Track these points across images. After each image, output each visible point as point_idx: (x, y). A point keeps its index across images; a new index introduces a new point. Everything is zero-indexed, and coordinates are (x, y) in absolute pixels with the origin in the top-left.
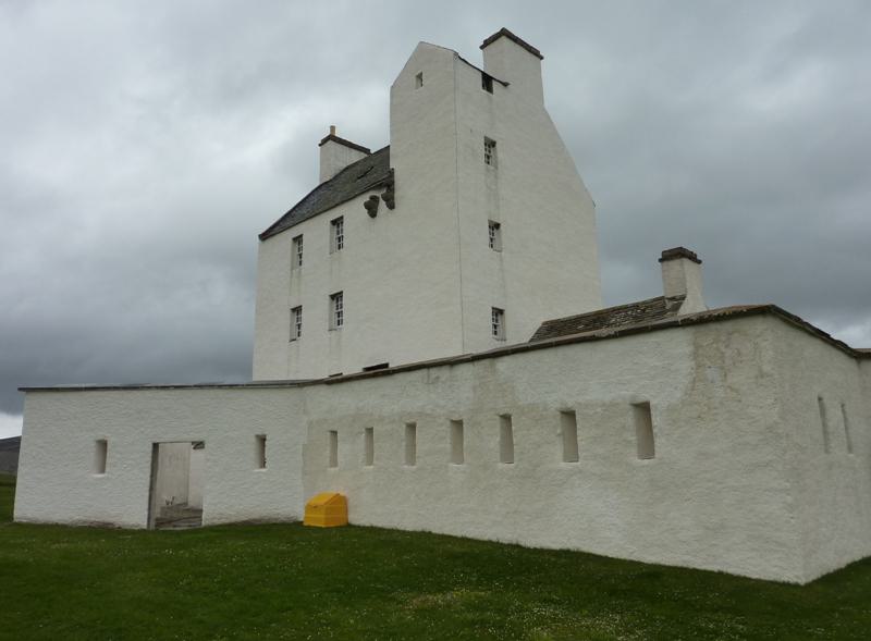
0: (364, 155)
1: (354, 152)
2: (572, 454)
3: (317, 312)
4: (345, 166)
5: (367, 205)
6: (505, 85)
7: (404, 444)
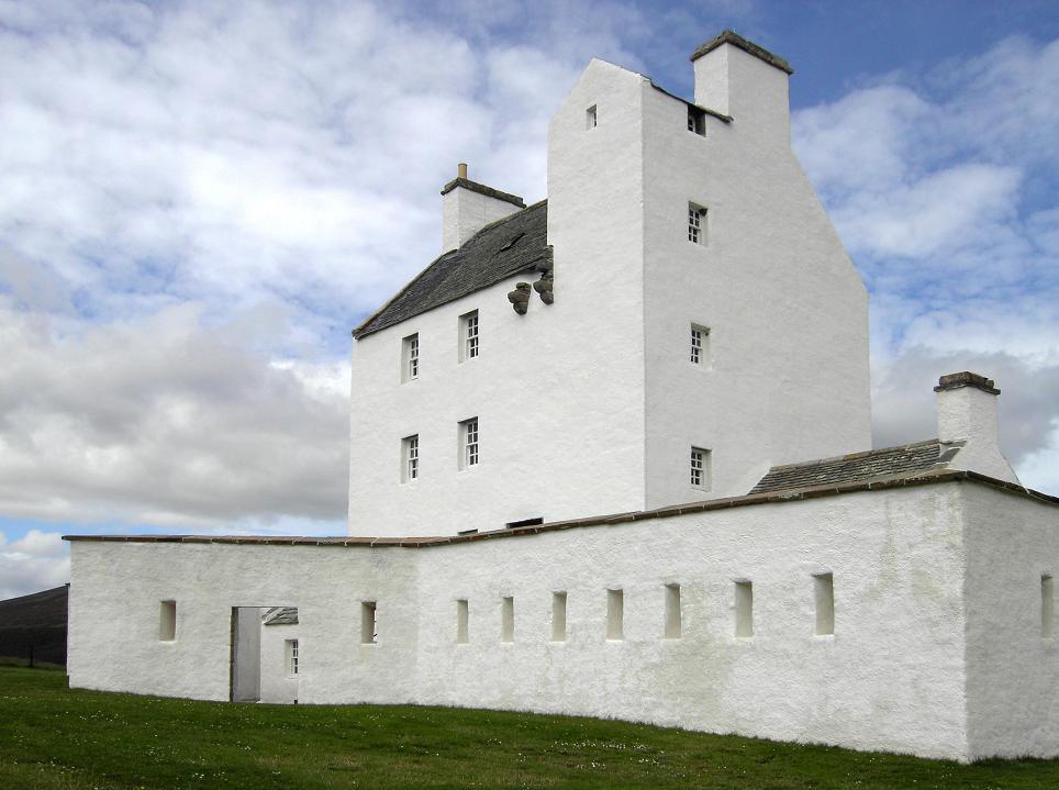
0: (512, 210)
1: (493, 203)
3: (442, 444)
4: (483, 226)
5: (512, 298)
6: (726, 120)
7: (551, 616)
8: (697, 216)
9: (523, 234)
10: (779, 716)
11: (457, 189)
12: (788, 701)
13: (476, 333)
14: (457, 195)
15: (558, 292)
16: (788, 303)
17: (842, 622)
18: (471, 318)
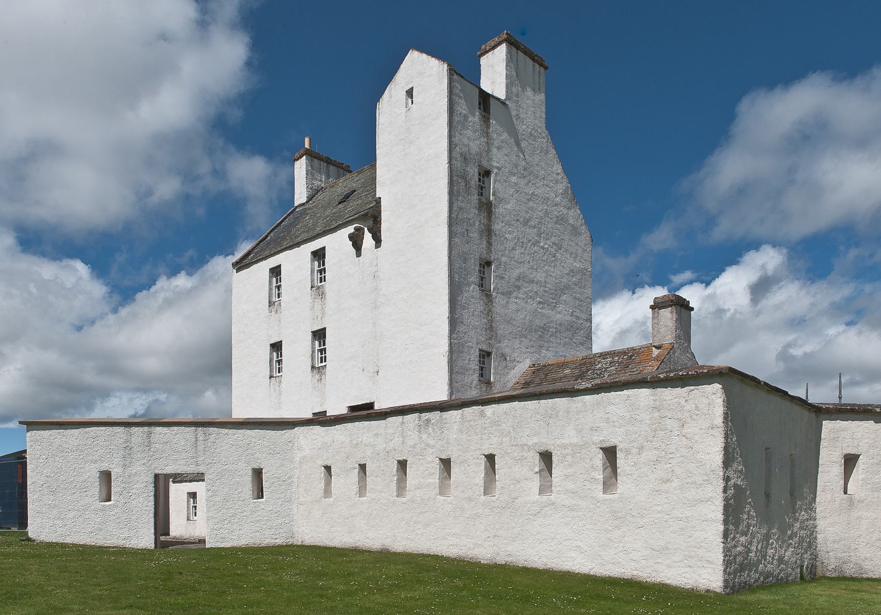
2: (545, 489)
5: (351, 237)
8: (483, 177)
9: (355, 191)
10: (573, 554)
12: (581, 544)
14: (505, 46)
16: (542, 244)
17: (624, 484)
18: (319, 255)
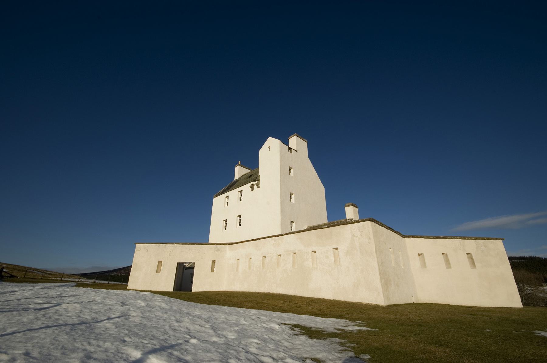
6: (296, 151)
11: (238, 166)
13: (242, 195)
14: (238, 168)
15: (261, 185)
